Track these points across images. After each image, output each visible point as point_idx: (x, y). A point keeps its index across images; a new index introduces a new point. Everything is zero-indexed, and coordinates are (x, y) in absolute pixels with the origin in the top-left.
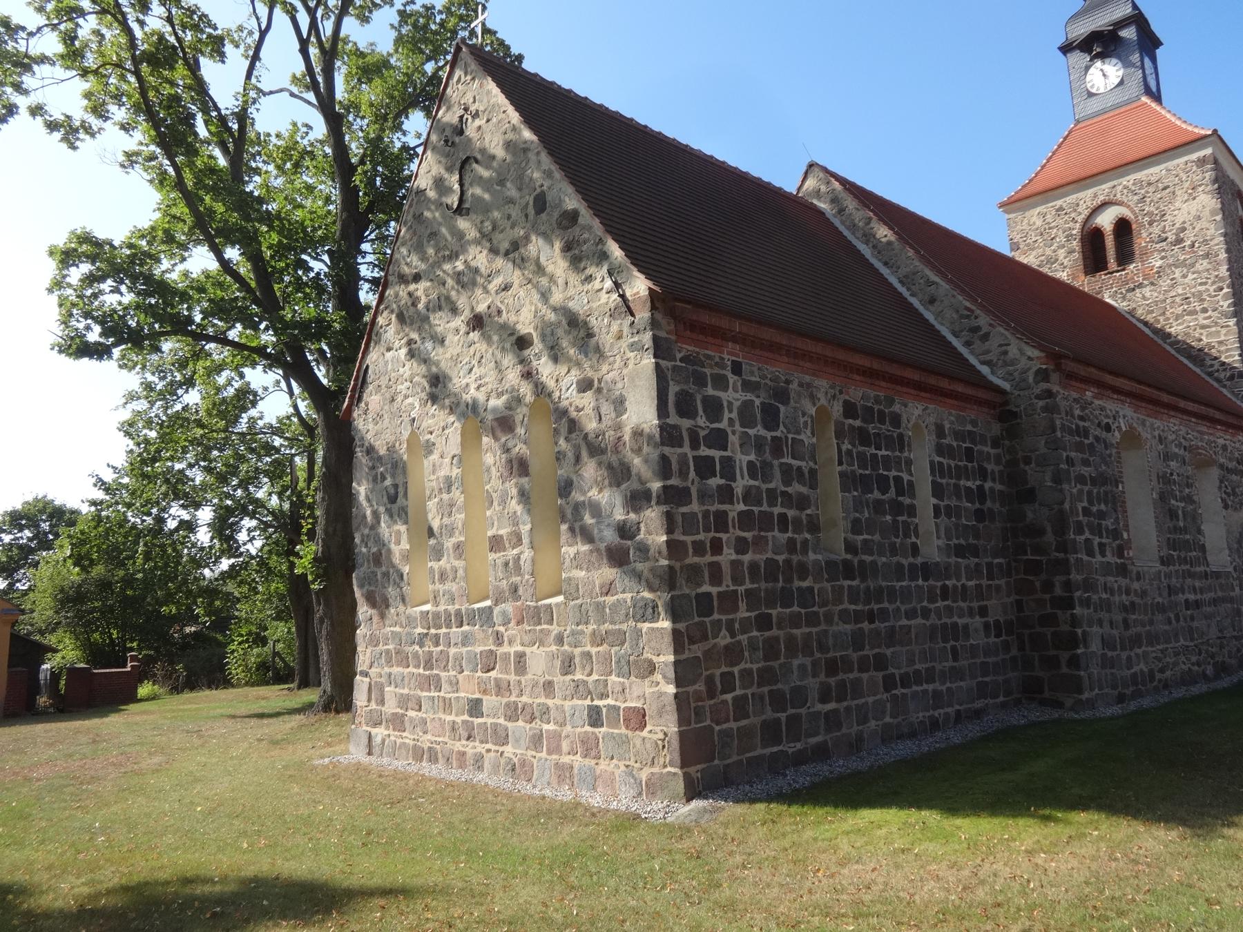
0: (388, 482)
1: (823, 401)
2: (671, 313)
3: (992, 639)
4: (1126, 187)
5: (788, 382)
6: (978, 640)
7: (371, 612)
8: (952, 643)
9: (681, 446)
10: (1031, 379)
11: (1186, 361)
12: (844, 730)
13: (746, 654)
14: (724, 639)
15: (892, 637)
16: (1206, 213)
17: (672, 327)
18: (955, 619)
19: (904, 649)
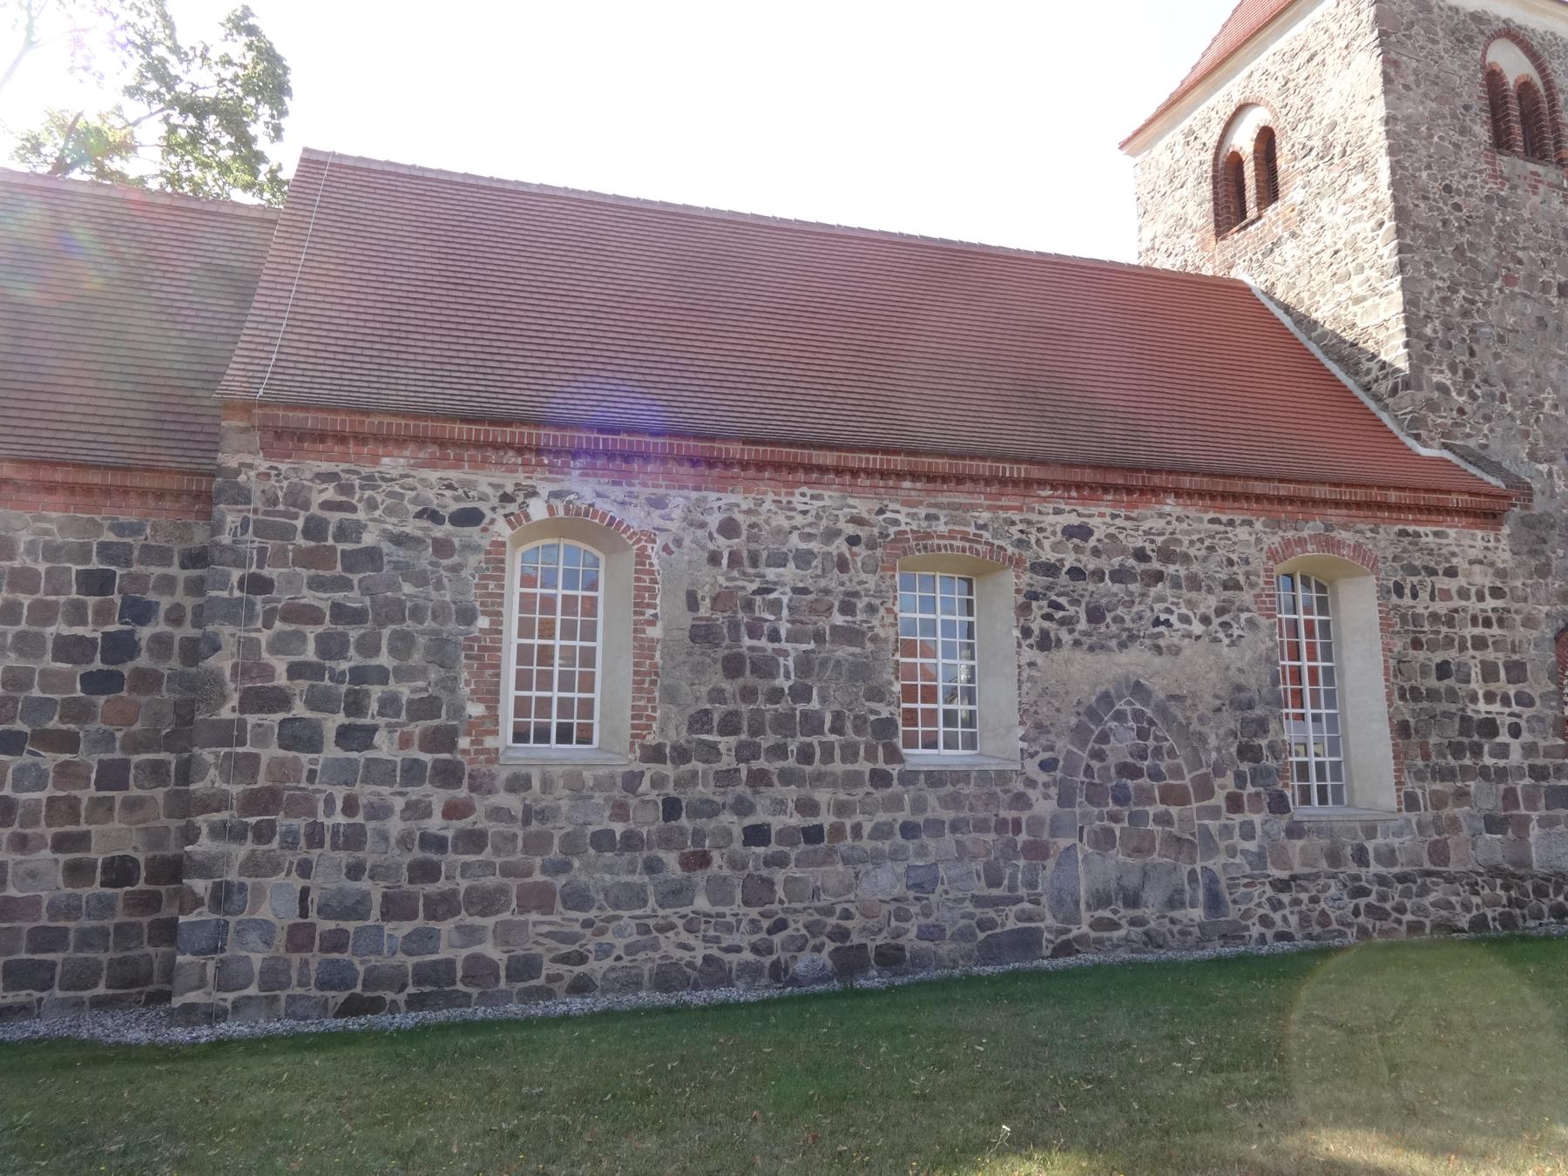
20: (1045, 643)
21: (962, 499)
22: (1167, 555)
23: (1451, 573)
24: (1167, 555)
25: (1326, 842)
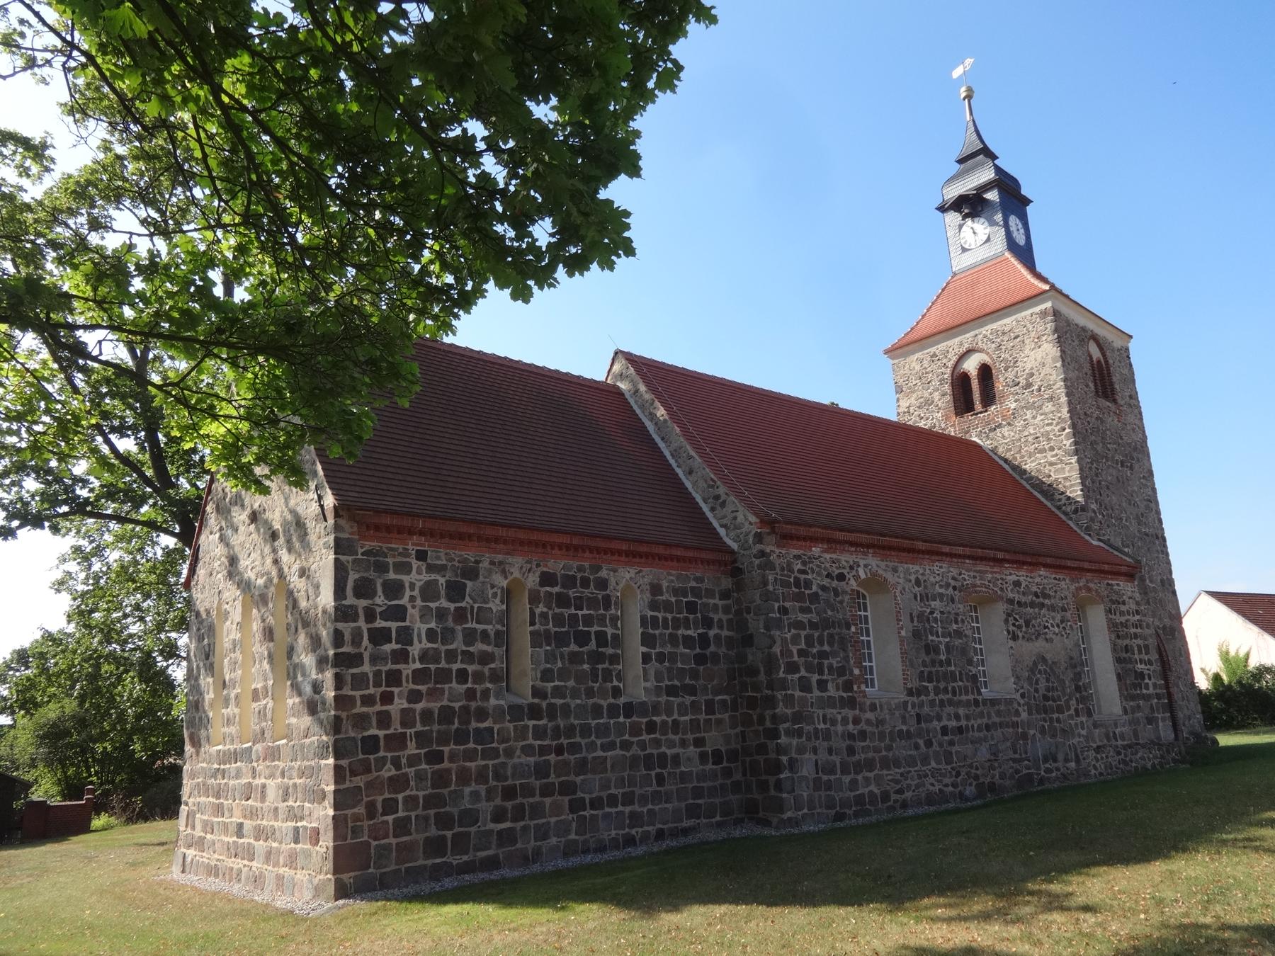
0: (206, 641)
1: (517, 574)
2: (352, 518)
3: (710, 766)
4: (985, 336)
5: (477, 562)
6: (696, 767)
7: (192, 750)
8: (658, 770)
9: (355, 621)
10: (751, 541)
11: (1039, 496)
12: (519, 845)
13: (412, 783)
14: (389, 772)
15: (582, 766)
16: (1049, 361)
17: (355, 529)
18: (663, 749)
19: (597, 777)
20: (1015, 638)
21: (983, 568)
22: (1046, 596)
23: (1124, 603)
24: (1046, 596)
25: (1103, 730)
